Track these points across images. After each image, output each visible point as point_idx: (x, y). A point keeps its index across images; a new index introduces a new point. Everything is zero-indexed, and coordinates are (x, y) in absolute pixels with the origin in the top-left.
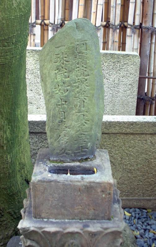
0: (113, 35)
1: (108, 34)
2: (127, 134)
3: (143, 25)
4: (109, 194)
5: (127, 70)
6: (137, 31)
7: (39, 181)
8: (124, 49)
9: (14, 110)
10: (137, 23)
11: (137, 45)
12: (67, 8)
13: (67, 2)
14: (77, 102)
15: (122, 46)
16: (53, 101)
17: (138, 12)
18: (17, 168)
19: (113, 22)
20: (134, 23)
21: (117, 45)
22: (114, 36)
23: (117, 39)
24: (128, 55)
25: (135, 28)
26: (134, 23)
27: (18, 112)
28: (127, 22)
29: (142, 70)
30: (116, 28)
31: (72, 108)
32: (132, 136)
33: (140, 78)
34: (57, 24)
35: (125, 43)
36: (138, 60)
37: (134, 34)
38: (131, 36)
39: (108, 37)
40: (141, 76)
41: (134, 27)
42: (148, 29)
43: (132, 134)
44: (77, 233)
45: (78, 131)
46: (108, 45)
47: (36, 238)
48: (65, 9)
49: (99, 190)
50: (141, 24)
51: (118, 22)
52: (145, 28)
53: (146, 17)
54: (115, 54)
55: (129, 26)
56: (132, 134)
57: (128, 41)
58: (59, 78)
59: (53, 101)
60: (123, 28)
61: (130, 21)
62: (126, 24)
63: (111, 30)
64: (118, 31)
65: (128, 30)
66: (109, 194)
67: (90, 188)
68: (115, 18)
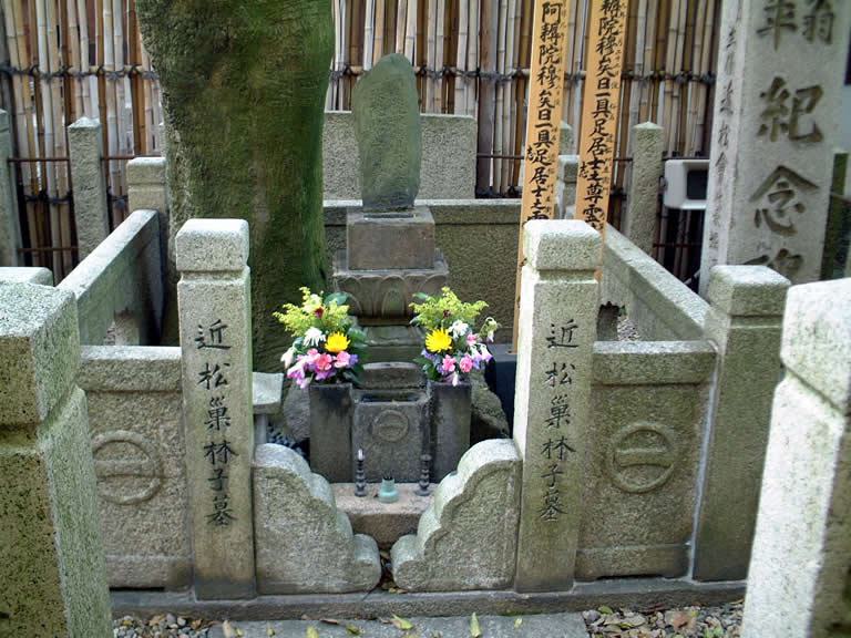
0: (432, 88)
1: (425, 87)
2: (455, 224)
3: (482, 71)
4: (431, 236)
5: (457, 145)
6: (473, 81)
7: (356, 223)
8: (451, 111)
9: (312, 168)
10: (472, 68)
11: (473, 105)
12: (354, 43)
13: (746, 7)
14: (394, 142)
15: (449, 106)
16: (368, 141)
17: (472, 49)
18: (312, 249)
19: (432, 66)
20: (466, 67)
21: (439, 105)
22: (434, 90)
23: (439, 96)
24: (457, 120)
25: (469, 76)
26: (466, 67)
27: (316, 171)
28: (455, 65)
29: (481, 145)
30: (437, 77)
31: (388, 149)
32: (463, 228)
33: (478, 157)
34: (338, 72)
35: (453, 103)
36: (474, 128)
37: (468, 86)
38: (463, 90)
39: (424, 92)
40: (480, 154)
41: (467, 75)
42: (490, 77)
43: (464, 224)
44: (398, 278)
45: (394, 174)
46: (424, 106)
47: (353, 289)
48: (350, 47)
49: (420, 232)
50: (478, 70)
51: (439, 67)
52: (485, 75)
53: (486, 57)
54: (437, 118)
55: (458, 73)
56: (464, 224)
57: (458, 97)
58: (374, 116)
59: (368, 141)
60: (449, 77)
61: (460, 64)
62: (453, 69)
63: (428, 80)
64: (440, 81)
65: (458, 80)
66: (431, 236)
67: (410, 229)
68: (435, 60)
